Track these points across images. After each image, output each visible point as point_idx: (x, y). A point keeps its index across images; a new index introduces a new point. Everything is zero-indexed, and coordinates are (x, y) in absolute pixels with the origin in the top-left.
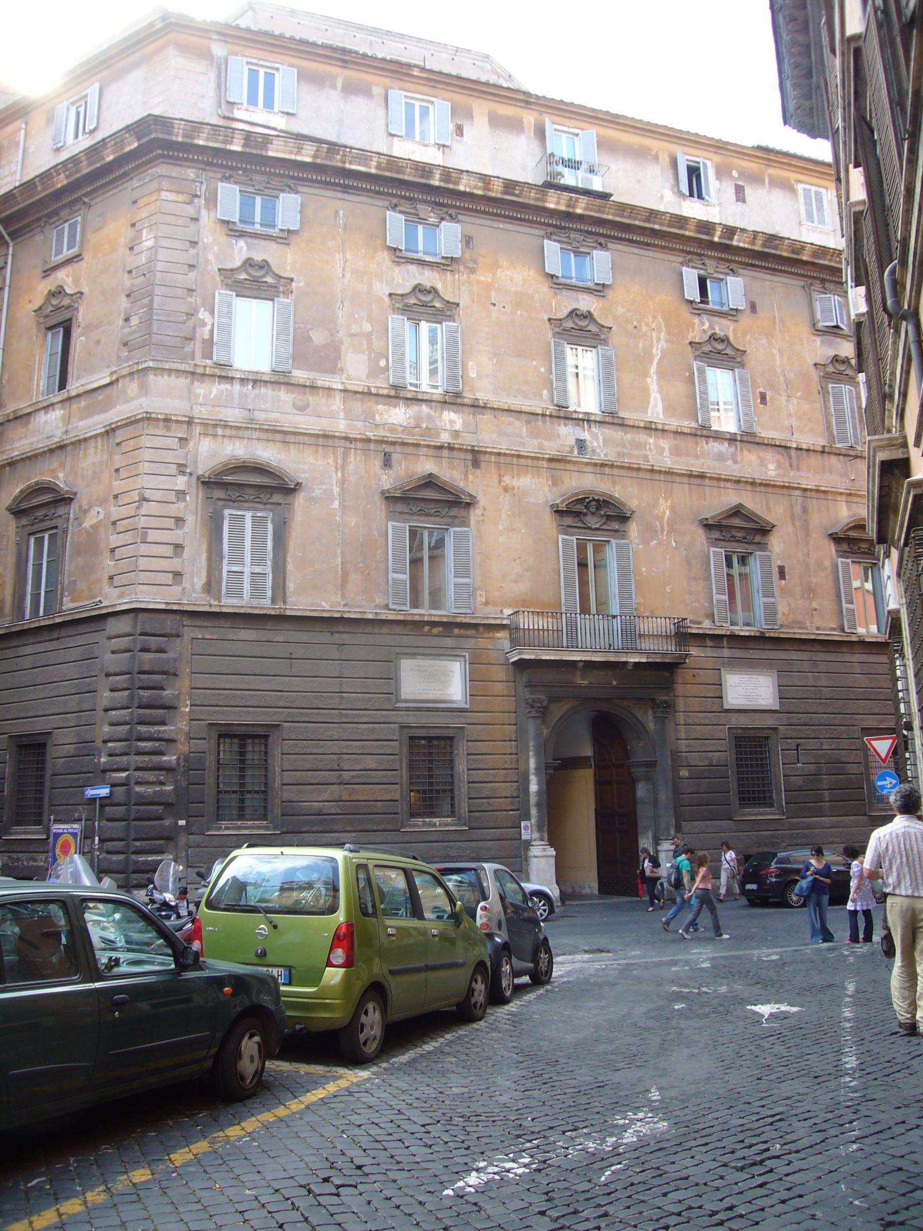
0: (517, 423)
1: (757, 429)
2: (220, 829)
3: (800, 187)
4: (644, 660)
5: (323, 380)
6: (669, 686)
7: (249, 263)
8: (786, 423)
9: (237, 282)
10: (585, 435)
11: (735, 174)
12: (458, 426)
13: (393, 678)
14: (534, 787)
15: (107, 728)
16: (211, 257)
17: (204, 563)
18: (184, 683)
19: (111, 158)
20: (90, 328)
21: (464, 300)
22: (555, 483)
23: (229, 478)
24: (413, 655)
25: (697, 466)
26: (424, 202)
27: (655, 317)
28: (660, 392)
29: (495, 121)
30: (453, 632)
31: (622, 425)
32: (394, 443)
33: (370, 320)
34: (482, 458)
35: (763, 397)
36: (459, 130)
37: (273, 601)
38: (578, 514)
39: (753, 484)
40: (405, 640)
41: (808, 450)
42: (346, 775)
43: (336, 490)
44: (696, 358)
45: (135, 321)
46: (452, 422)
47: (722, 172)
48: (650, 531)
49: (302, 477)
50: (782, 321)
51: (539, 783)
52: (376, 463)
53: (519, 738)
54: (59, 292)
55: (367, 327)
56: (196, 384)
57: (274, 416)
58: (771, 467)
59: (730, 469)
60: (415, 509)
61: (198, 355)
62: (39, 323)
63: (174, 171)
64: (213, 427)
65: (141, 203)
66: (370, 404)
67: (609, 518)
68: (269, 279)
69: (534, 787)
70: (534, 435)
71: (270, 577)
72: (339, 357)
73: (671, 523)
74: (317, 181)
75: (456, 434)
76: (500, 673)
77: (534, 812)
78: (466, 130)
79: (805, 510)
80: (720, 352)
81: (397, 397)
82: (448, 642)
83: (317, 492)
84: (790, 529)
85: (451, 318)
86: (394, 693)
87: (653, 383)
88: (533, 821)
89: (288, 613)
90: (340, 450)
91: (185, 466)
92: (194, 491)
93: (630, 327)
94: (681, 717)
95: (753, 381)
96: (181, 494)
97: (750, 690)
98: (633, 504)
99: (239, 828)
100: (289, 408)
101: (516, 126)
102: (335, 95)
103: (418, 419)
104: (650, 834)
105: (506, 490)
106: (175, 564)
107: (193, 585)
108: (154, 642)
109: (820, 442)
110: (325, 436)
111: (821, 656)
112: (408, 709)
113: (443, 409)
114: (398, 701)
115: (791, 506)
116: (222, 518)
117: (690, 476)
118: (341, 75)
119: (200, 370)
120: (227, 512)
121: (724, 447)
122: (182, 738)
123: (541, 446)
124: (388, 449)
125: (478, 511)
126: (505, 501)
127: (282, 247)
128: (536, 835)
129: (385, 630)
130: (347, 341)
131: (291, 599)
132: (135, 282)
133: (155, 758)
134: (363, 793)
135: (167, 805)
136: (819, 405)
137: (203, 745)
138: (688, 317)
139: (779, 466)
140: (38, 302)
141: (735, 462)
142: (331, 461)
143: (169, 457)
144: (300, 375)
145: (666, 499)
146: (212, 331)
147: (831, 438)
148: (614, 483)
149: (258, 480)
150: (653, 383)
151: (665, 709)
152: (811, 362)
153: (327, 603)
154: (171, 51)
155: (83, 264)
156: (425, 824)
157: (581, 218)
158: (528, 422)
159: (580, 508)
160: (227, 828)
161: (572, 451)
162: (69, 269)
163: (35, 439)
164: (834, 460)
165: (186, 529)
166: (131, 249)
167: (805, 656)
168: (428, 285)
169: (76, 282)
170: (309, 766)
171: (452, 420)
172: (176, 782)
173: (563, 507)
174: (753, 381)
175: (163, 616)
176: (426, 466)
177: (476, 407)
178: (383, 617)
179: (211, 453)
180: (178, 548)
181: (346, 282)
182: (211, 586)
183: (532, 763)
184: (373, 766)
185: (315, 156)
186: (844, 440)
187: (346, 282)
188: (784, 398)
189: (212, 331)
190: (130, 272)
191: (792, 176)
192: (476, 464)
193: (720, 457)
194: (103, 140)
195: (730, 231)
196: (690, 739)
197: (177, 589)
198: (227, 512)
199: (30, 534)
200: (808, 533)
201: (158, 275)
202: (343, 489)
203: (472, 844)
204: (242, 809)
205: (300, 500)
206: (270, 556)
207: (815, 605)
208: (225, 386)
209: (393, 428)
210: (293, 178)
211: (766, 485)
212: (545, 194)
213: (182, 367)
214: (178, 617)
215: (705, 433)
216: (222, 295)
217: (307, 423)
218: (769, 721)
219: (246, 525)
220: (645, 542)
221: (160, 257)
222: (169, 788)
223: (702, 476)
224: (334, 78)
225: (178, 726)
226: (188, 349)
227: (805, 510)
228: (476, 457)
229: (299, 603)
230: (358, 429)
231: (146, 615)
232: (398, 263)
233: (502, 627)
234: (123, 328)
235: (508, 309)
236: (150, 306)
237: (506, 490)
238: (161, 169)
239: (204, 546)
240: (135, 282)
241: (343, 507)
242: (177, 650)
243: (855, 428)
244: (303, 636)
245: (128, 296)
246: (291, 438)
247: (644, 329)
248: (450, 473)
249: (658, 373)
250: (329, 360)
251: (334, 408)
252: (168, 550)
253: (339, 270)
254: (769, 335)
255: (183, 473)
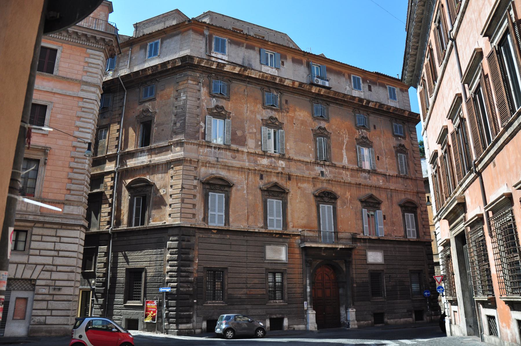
0: (302, 165)
1: (376, 168)
2: (207, 303)
3: (388, 86)
4: (344, 247)
5: (240, 149)
6: (350, 255)
7: (217, 107)
8: (385, 167)
9: (213, 113)
10: (324, 170)
11: (368, 81)
12: (284, 166)
13: (264, 252)
14: (308, 290)
15: (168, 267)
16: (204, 104)
17: (202, 211)
18: (196, 253)
19: (170, 67)
20: (158, 125)
21: (285, 122)
22: (314, 186)
23: (211, 182)
24: (270, 244)
25: (359, 181)
26: (273, 88)
27: (344, 130)
28: (346, 155)
29: (294, 61)
30: (280, 238)
31: (334, 166)
32: (263, 171)
33: (256, 128)
34: (292, 177)
35: (378, 157)
36: (283, 63)
37: (225, 225)
38: (322, 197)
39: (376, 187)
40: (268, 239)
41: (392, 176)
42: (249, 285)
43: (245, 187)
44: (358, 144)
45: (178, 125)
46: (282, 164)
47: (364, 81)
48: (344, 203)
49: (235, 182)
50: (383, 132)
51: (310, 289)
52: (258, 178)
53: (303, 273)
54: (148, 110)
55: (255, 130)
56: (200, 148)
57: (225, 160)
58: (381, 181)
59: (369, 182)
60: (271, 194)
61: (200, 138)
62: (138, 121)
63: (193, 74)
64: (205, 164)
65: (180, 83)
66: (256, 157)
67: (331, 198)
68: (223, 112)
69: (308, 290)
70: (308, 169)
71: (224, 216)
72: (246, 140)
73: (350, 200)
74: (238, 79)
75: (283, 168)
76: (297, 251)
77: (308, 298)
78: (285, 63)
79: (391, 196)
80: (365, 142)
81: (264, 155)
82: (281, 240)
83: (239, 187)
84: (387, 203)
85: (281, 128)
86: (264, 257)
87: (344, 152)
88: (308, 301)
89: (231, 229)
90: (247, 173)
91: (196, 177)
92: (199, 185)
93: (337, 133)
94: (354, 267)
95: (375, 152)
96: (195, 187)
97: (375, 257)
98: (339, 193)
99: (214, 303)
100: (230, 158)
101: (300, 62)
102: (243, 49)
103: (271, 162)
104: (344, 306)
105: (299, 188)
106: (193, 211)
107: (199, 218)
108: (186, 238)
109: (396, 173)
110: (242, 168)
111: (397, 246)
112: (268, 263)
113: (279, 160)
114: (265, 260)
115: (387, 195)
116: (208, 195)
117: (356, 184)
118: (246, 43)
119: (201, 144)
120: (210, 193)
121: (366, 175)
122: (195, 272)
123: (310, 174)
124: (262, 173)
125: (290, 195)
126: (299, 192)
127: (227, 101)
128: (309, 306)
129: (261, 235)
130: (248, 135)
131: (231, 224)
132: (178, 111)
133: (187, 279)
134: (254, 292)
135: (190, 295)
136: (395, 161)
137: (202, 274)
138: (355, 130)
139: (383, 181)
140: (137, 113)
141: (370, 180)
142: (243, 176)
143: (191, 173)
144: (234, 146)
145: (349, 192)
146: (205, 130)
147: (399, 173)
148: (333, 187)
149: (221, 183)
150: (344, 152)
151: (348, 263)
152: (392, 146)
153: (242, 226)
154: (191, 32)
155: (156, 102)
156: (274, 302)
157: (322, 95)
158: (306, 165)
159: (322, 195)
160: (210, 303)
161: (319, 175)
162: (150, 103)
163: (136, 162)
164: (400, 179)
165: (197, 199)
166: (176, 99)
167: (392, 245)
168: (274, 117)
169: (153, 108)
170: (236, 282)
171: (282, 163)
172: (193, 287)
173: (317, 195)
174: (375, 152)
175: (189, 229)
176: (274, 179)
177: (290, 159)
178: (261, 231)
179: (204, 172)
180: (194, 205)
181: (248, 114)
182: (205, 219)
183: (308, 281)
184: (257, 282)
185: (239, 71)
186: (403, 173)
187: (248, 114)
188: (384, 158)
189: (205, 130)
190: (176, 107)
191: (386, 83)
192: (290, 179)
193: (365, 178)
194: (168, 61)
195: (369, 102)
196: (358, 275)
197: (194, 220)
198: (210, 193)
199: (135, 196)
200: (392, 204)
201: (187, 109)
202: (247, 186)
203: (289, 309)
204: (214, 296)
205: (234, 189)
206: (224, 209)
207: (395, 228)
208: (209, 149)
209: (263, 166)
210: (231, 78)
211: (380, 188)
212: (312, 87)
213: (196, 142)
214: (194, 230)
215: (361, 170)
216: (208, 117)
217: (236, 163)
218: (381, 268)
219: (216, 198)
220: (342, 207)
221: (188, 103)
222: (191, 289)
223: (360, 184)
224: (243, 43)
225: (195, 267)
226: (197, 136)
227: (391, 196)
228: (289, 177)
229: (233, 226)
230: (252, 166)
231: (184, 228)
232: (264, 109)
233: (298, 235)
234: (173, 126)
235: (299, 125)
236: (185, 120)
237: (299, 188)
238: (189, 73)
239: (203, 205)
240: (178, 111)
241: (247, 193)
242: (193, 240)
243: (406, 169)
244: (234, 237)
245: (175, 115)
246: (231, 168)
247: (341, 133)
248: (282, 182)
249: (346, 149)
250: (242, 142)
251: (245, 158)
252: (191, 206)
253: (245, 111)
254: (380, 137)
255: (196, 179)
